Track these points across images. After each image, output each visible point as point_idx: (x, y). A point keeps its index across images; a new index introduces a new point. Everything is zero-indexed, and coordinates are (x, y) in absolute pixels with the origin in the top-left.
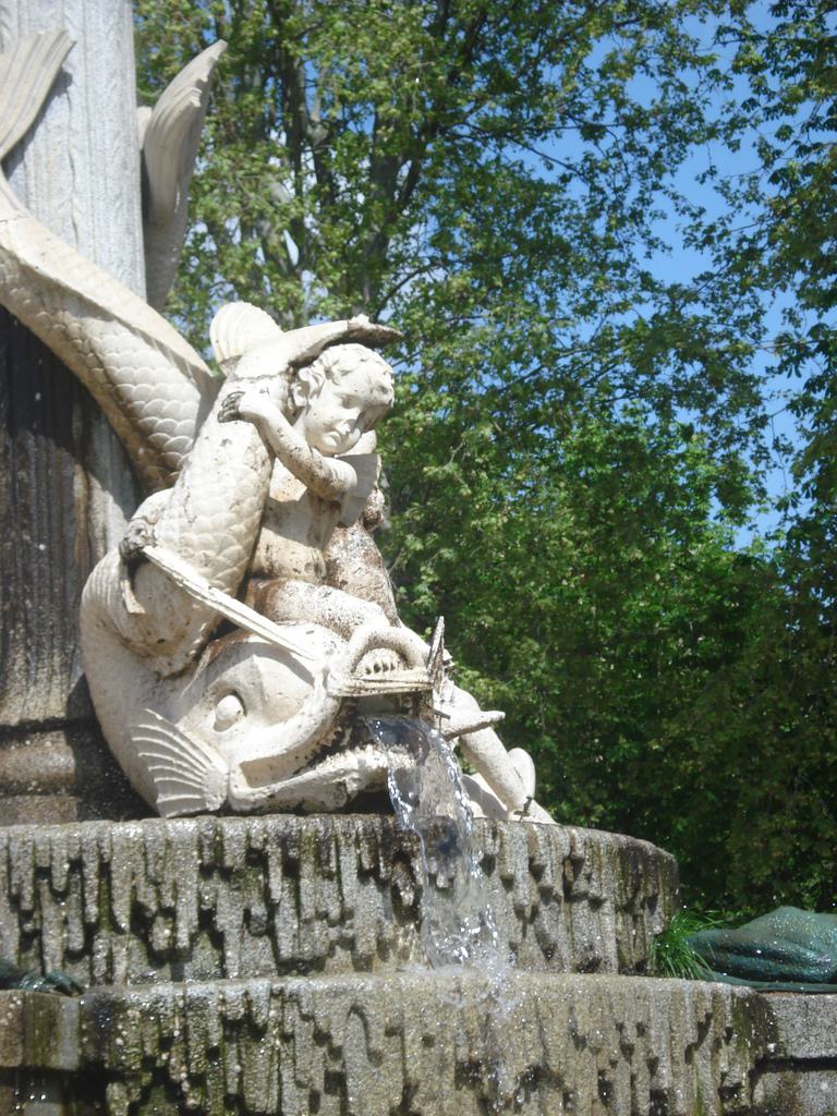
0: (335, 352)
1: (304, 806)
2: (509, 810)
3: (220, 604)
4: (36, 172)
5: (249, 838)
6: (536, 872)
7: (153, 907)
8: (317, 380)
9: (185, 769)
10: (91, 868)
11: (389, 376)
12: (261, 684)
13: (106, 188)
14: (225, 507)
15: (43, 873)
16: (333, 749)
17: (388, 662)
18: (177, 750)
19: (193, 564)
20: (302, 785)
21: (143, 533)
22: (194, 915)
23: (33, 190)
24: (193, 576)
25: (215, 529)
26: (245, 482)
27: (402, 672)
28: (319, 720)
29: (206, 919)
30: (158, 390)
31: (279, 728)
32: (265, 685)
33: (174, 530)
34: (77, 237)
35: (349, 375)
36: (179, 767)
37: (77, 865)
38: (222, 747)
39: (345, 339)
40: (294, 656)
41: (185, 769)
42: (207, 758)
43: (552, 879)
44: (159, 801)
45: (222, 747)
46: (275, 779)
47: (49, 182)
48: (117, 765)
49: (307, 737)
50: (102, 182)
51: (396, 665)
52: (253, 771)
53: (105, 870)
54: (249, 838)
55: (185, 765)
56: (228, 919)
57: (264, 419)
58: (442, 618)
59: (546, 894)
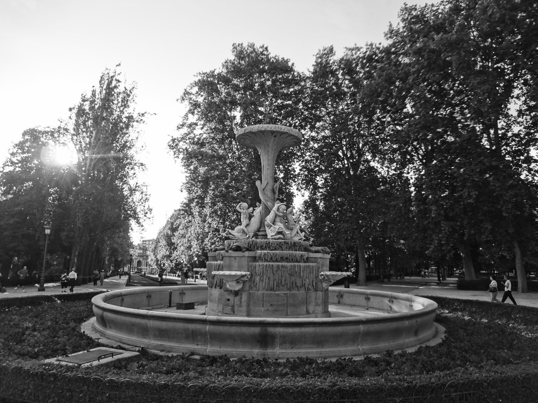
52: (272, 236)
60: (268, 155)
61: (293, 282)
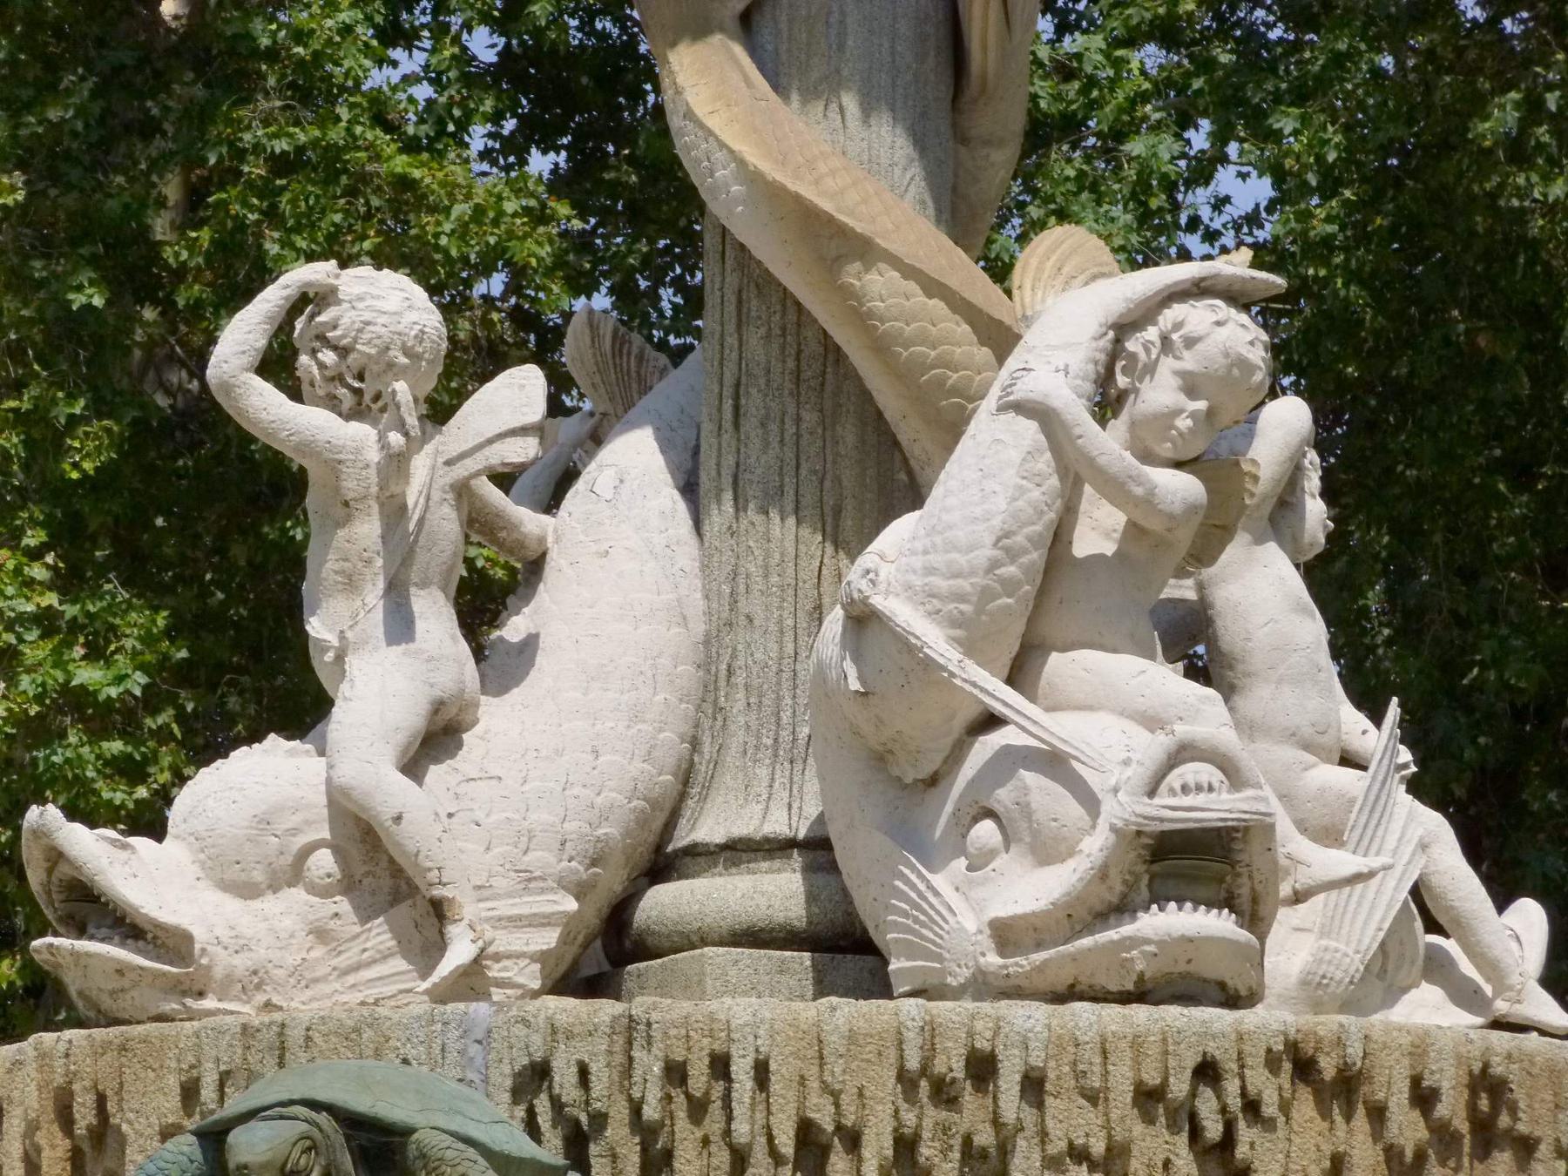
0: (1176, 312)
1: (1078, 988)
2: (1497, 994)
3: (974, 685)
4: (790, 29)
5: (971, 1034)
6: (1424, 1098)
7: (830, 1128)
8: (1147, 351)
9: (923, 925)
10: (742, 1070)
11: (1260, 347)
12: (1028, 805)
13: (893, 54)
14: (989, 540)
15: (676, 1073)
16: (1122, 909)
17: (1204, 780)
18: (913, 895)
19: (939, 623)
20: (1074, 958)
21: (871, 575)
22: (888, 1142)
23: (784, 57)
24: (936, 641)
25: (972, 573)
26: (1020, 503)
27: (1225, 796)
28: (1099, 862)
30: (938, 357)
31: (1071, 863)
32: (1034, 806)
33: (914, 572)
34: (845, 127)
35: (1199, 347)
36: (916, 920)
37: (720, 1066)
38: (973, 894)
39: (1198, 290)
40: (1075, 764)
41: (923, 925)
42: (950, 909)
43: (1452, 1107)
44: (891, 967)
45: (973, 894)
46: (1039, 946)
47: (809, 44)
48: (851, 903)
49: (1080, 886)
50: (886, 45)
51: (1216, 785)
52: (1006, 935)
53: (762, 1072)
54: (971, 1034)
55: (922, 917)
57: (1054, 410)
58: (1395, 700)
59: (1444, 1137)
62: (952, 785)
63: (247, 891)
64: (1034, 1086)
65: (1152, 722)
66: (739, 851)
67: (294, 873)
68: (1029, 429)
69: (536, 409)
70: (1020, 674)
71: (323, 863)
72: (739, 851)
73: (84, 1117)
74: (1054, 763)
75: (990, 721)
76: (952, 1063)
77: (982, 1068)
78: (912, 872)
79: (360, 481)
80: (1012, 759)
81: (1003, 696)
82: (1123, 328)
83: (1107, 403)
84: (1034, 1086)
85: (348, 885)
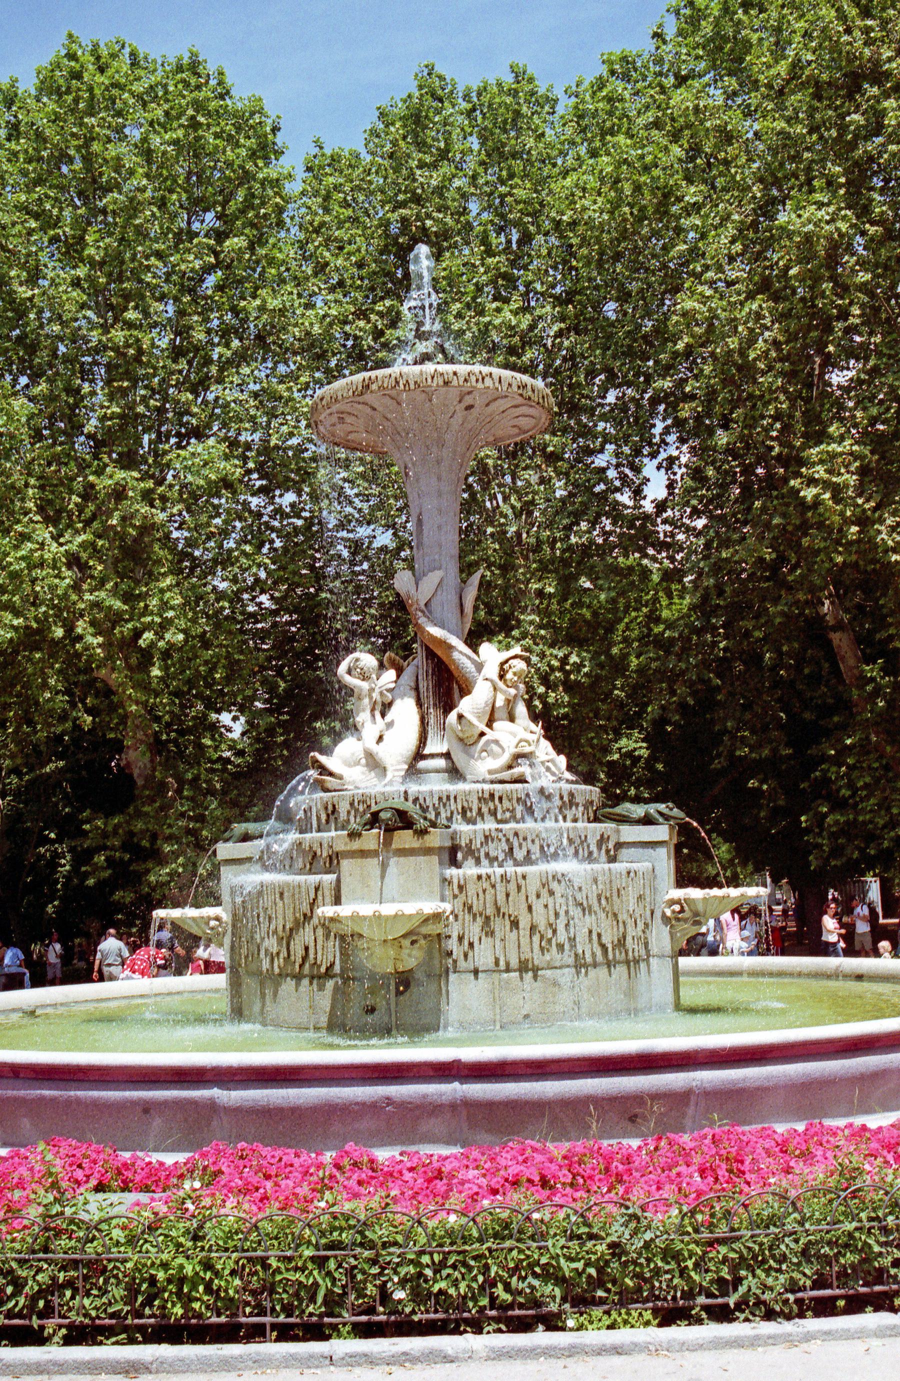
15: (440, 799)
24: (475, 721)
29: (480, 809)
37: (448, 798)
43: (566, 799)
52: (490, 772)
56: (485, 810)
60: (439, 479)
61: (590, 932)
62: (767, 1078)
63: (350, 766)
64: (501, 799)
65: (515, 735)
66: (432, 756)
67: (358, 763)
68: (489, 684)
69: (394, 678)
70: (489, 725)
71: (363, 761)
72: (432, 756)
73: (330, 808)
74: (496, 742)
75: (482, 734)
76: (486, 795)
77: (492, 796)
78: (472, 762)
79: (365, 692)
80: (488, 743)
81: (486, 730)
82: (502, 664)
83: (501, 677)
84: (501, 799)
85: (367, 765)
